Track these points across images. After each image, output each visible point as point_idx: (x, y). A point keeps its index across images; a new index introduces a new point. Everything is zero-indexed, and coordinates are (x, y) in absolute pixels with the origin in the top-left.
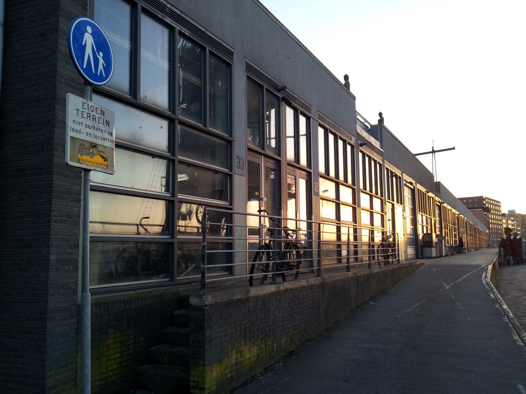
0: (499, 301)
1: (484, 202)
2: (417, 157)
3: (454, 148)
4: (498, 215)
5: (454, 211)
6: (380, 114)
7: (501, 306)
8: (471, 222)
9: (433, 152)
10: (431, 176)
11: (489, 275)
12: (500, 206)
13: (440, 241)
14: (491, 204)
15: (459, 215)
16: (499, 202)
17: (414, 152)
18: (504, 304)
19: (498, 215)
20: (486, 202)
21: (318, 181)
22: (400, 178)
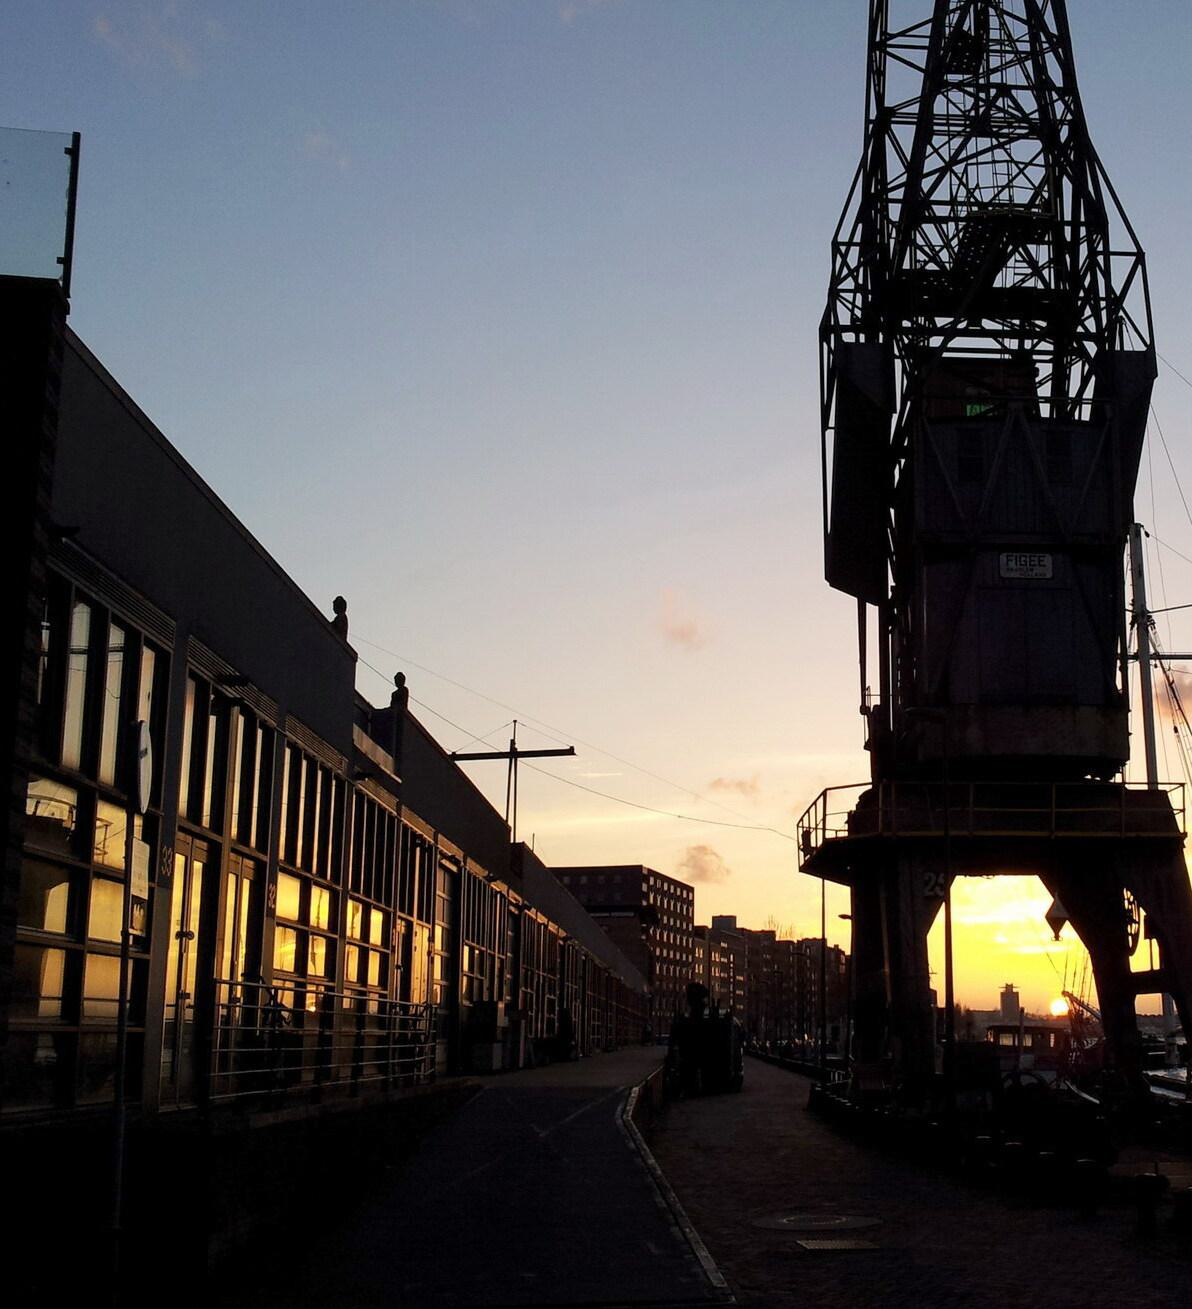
0: (643, 1153)
1: (645, 887)
2: (460, 763)
3: (570, 752)
4: (684, 932)
5: (552, 927)
6: (400, 679)
7: (644, 1161)
8: (597, 961)
9: (513, 754)
10: (502, 828)
11: (630, 1108)
12: (691, 903)
13: (514, 1025)
14: (664, 894)
15: (565, 939)
16: (691, 890)
17: (449, 748)
18: (651, 1156)
19: (684, 932)
20: (650, 888)
21: (274, 882)
22: (430, 846)
